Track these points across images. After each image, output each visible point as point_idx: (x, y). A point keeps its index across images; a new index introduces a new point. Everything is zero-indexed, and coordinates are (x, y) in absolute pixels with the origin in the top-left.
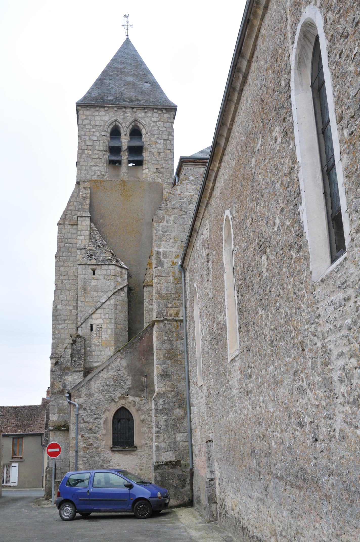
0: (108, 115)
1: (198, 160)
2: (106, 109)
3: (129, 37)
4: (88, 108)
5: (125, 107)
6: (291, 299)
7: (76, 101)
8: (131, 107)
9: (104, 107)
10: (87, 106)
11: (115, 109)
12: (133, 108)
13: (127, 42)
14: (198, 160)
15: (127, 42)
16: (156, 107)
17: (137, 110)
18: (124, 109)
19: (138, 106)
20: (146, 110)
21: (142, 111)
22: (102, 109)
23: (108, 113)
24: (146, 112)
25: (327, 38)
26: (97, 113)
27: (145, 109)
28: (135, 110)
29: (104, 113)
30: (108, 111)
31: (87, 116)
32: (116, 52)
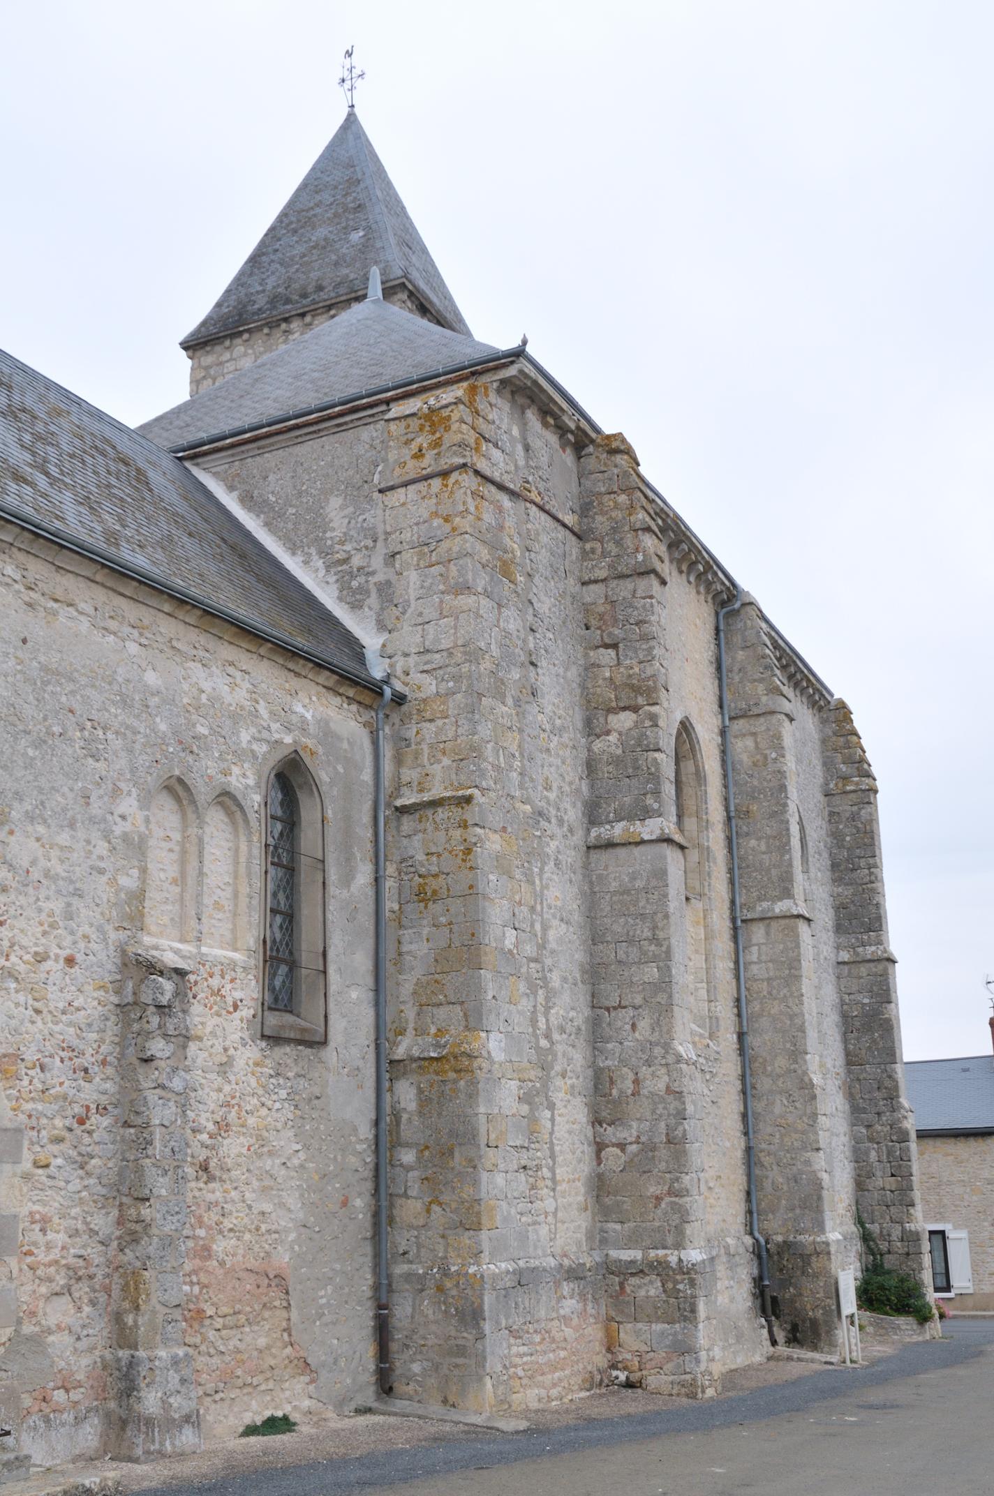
0: (250, 351)
1: (351, 425)
2: (246, 336)
3: (356, 110)
4: (208, 348)
5: (286, 320)
6: (89, 1219)
7: (181, 338)
8: (298, 315)
9: (240, 333)
10: (205, 344)
11: (266, 330)
12: (303, 315)
13: (351, 121)
14: (351, 425)
15: (351, 121)
16: (353, 295)
17: (313, 316)
18: (284, 326)
19: (312, 307)
20: (332, 312)
21: (325, 316)
22: (238, 341)
23: (252, 347)
24: (333, 317)
25: (669, 947)
26: (227, 356)
27: (330, 307)
28: (308, 319)
29: (242, 349)
30: (251, 342)
31: (207, 368)
32: (310, 166)
